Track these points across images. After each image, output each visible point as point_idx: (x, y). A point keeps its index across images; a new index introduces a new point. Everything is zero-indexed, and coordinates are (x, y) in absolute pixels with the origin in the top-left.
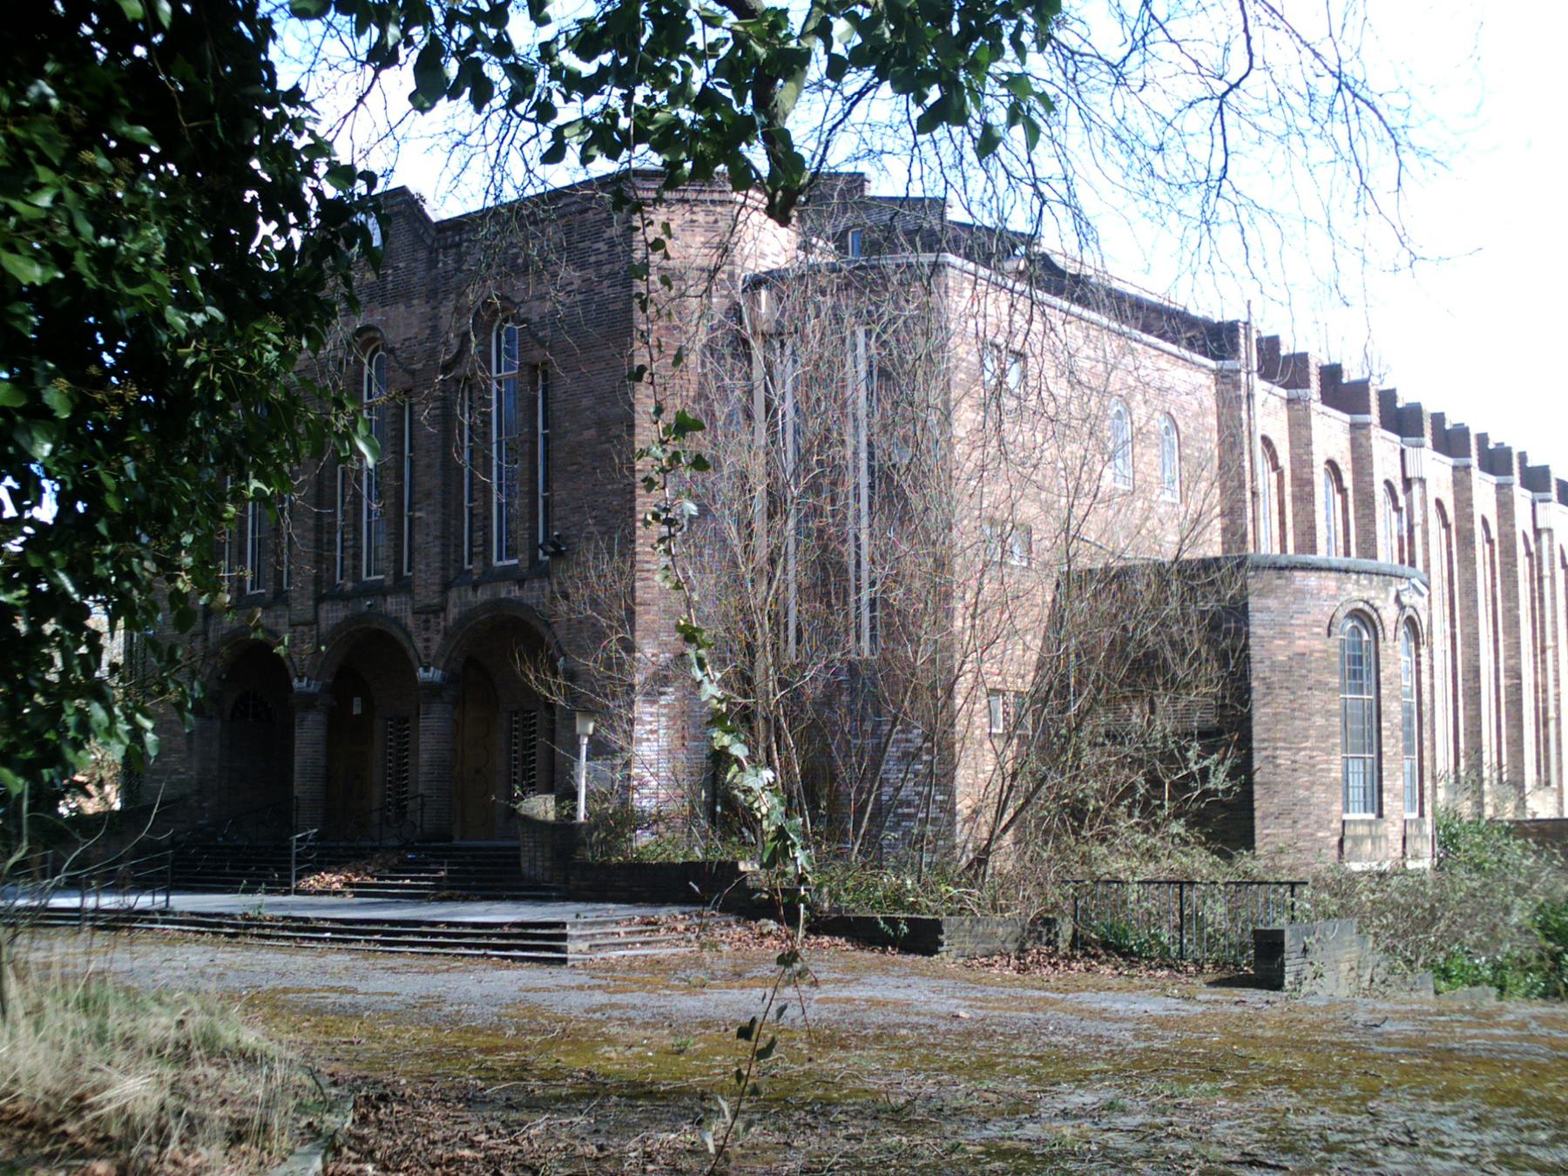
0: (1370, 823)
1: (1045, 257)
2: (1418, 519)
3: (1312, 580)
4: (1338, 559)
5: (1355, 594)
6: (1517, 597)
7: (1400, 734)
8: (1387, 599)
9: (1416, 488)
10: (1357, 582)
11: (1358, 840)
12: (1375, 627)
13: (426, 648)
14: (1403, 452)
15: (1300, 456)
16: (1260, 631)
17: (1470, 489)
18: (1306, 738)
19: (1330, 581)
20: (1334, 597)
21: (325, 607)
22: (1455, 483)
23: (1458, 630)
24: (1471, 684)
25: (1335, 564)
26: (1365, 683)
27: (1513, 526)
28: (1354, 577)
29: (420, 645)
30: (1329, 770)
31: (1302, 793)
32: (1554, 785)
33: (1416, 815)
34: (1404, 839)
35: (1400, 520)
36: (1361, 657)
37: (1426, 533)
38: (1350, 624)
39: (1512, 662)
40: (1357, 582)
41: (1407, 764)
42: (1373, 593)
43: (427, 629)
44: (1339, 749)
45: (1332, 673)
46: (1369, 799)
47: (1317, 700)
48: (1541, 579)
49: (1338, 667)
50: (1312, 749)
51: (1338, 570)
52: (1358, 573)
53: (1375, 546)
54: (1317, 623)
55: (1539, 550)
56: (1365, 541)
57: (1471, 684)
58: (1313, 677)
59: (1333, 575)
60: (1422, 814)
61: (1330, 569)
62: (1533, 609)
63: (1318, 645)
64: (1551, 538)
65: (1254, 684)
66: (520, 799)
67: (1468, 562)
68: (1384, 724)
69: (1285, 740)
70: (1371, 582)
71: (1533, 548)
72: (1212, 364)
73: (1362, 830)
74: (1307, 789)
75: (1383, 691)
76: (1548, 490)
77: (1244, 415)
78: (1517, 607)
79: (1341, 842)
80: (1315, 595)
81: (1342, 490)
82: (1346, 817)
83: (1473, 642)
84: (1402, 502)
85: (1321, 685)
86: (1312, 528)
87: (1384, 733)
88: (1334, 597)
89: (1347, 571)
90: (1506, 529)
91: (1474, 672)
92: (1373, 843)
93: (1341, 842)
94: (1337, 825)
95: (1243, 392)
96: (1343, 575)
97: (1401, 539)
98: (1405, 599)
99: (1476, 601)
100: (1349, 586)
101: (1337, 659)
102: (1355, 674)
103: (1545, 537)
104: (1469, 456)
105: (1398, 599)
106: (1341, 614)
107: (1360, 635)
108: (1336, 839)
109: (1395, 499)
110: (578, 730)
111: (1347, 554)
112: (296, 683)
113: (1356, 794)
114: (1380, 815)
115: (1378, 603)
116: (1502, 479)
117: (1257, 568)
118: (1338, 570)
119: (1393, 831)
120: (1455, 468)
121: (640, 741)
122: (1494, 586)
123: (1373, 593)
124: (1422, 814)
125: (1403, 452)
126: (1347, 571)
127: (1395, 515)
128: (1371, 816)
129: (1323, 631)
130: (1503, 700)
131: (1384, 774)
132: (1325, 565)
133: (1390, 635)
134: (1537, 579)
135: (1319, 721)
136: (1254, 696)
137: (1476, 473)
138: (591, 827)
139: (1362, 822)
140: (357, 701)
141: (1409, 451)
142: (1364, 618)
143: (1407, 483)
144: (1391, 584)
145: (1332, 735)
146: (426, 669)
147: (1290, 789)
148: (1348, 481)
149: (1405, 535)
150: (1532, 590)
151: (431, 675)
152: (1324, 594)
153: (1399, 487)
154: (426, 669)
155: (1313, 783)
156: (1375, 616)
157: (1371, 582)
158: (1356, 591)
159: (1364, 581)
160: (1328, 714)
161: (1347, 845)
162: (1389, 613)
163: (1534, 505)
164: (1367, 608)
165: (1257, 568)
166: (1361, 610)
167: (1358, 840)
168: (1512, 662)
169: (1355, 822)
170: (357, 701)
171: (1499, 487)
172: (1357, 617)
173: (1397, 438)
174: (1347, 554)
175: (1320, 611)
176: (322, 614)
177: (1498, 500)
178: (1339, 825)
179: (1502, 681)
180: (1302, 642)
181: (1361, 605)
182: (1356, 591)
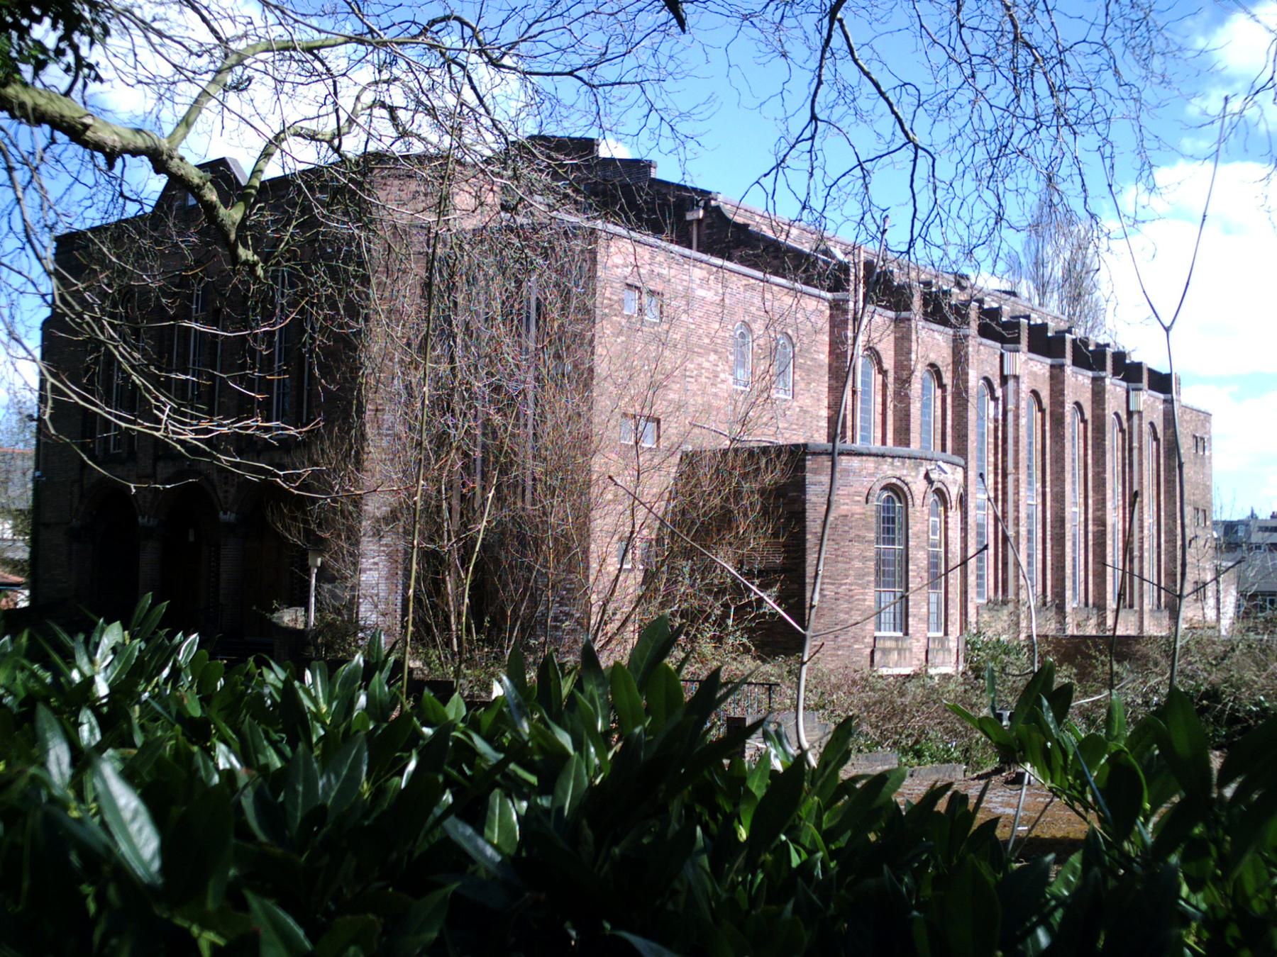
0: (897, 639)
1: (718, 208)
2: (1011, 406)
3: (855, 462)
4: (876, 446)
5: (889, 473)
6: (1104, 464)
7: (925, 575)
8: (918, 474)
9: (1011, 383)
10: (892, 463)
11: (885, 651)
12: (906, 497)
13: (226, 497)
14: (1002, 356)
15: (902, 362)
16: (814, 499)
17: (1063, 382)
18: (847, 576)
19: (870, 463)
20: (872, 475)
21: (161, 464)
22: (1052, 377)
23: (1048, 490)
24: (1057, 530)
25: (874, 451)
26: (897, 536)
27: (1104, 409)
28: (890, 460)
29: (221, 495)
30: (865, 600)
31: (842, 616)
32: (1136, 608)
33: (941, 634)
34: (927, 652)
35: (996, 407)
36: (893, 519)
37: (1017, 417)
38: (885, 494)
39: (1099, 513)
40: (892, 463)
41: (933, 598)
42: (905, 472)
43: (226, 484)
44: (872, 585)
45: (869, 530)
46: (898, 621)
47: (856, 549)
48: (1131, 449)
49: (874, 526)
50: (851, 584)
51: (876, 455)
52: (893, 457)
53: (967, 428)
54: (858, 494)
55: (1130, 427)
56: (959, 424)
57: (1057, 530)
58: (852, 534)
59: (872, 459)
60: (946, 634)
61: (869, 455)
62: (1124, 472)
63: (857, 509)
64: (1141, 418)
65: (808, 536)
66: (277, 610)
67: (1058, 437)
68: (910, 567)
69: (830, 577)
70: (904, 464)
71: (1125, 425)
72: (829, 295)
73: (889, 644)
74: (847, 613)
75: (911, 543)
76: (1140, 381)
77: (850, 334)
78: (1104, 472)
79: (872, 653)
80: (857, 474)
81: (942, 386)
82: (877, 634)
83: (1059, 498)
84: (999, 393)
85: (859, 538)
86: (908, 415)
87: (911, 574)
88: (872, 475)
89: (883, 456)
90: (1099, 412)
91: (1060, 521)
92: (899, 654)
93: (872, 653)
94: (869, 640)
95: (850, 316)
96: (880, 459)
97: (996, 420)
98: (933, 476)
99: (1063, 468)
100: (885, 467)
101: (874, 520)
102: (888, 531)
103: (1136, 417)
104: (1064, 357)
105: (927, 476)
106: (877, 488)
107: (893, 502)
108: (869, 650)
109: (992, 390)
110: (310, 562)
111: (884, 442)
112: (140, 519)
113: (887, 617)
114: (906, 634)
115: (908, 479)
116: (1096, 374)
117: (814, 454)
118: (876, 455)
119: (917, 647)
120: (1052, 366)
121: (365, 571)
122: (1086, 455)
123: (905, 472)
124: (946, 634)
125: (1002, 356)
126: (883, 456)
127: (992, 404)
128: (900, 634)
129: (863, 499)
130: (1090, 543)
131: (910, 603)
132: (865, 451)
133: (918, 502)
134: (1128, 450)
135: (857, 564)
136: (808, 545)
137: (1069, 370)
138: (319, 632)
139: (890, 638)
140: (191, 532)
141: (1007, 355)
142: (897, 491)
143: (1004, 380)
144: (921, 465)
145: (868, 574)
146: (225, 513)
147: (833, 613)
148: (947, 379)
149: (1000, 417)
150: (1124, 459)
151: (228, 517)
152: (864, 473)
153: (996, 383)
154: (225, 513)
155: (851, 609)
156: (906, 489)
157: (904, 464)
158: (890, 471)
159: (897, 462)
160: (865, 559)
161: (877, 656)
162: (918, 486)
163: (1128, 393)
164: (899, 483)
165: (814, 454)
166: (894, 484)
167: (885, 651)
168: (1099, 513)
169: (884, 638)
170: (191, 532)
171: (1094, 380)
172: (892, 490)
173: (999, 345)
174: (884, 442)
175: (861, 485)
176: (159, 470)
177: (1093, 390)
178: (871, 640)
179: (1090, 528)
180: (845, 507)
181: (894, 480)
182: (890, 471)
